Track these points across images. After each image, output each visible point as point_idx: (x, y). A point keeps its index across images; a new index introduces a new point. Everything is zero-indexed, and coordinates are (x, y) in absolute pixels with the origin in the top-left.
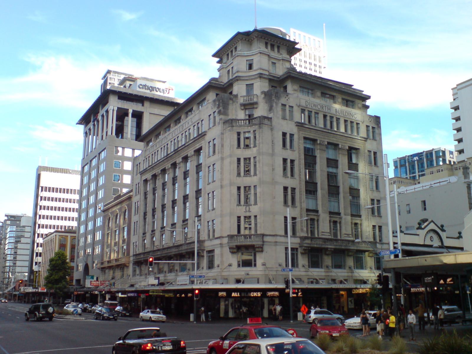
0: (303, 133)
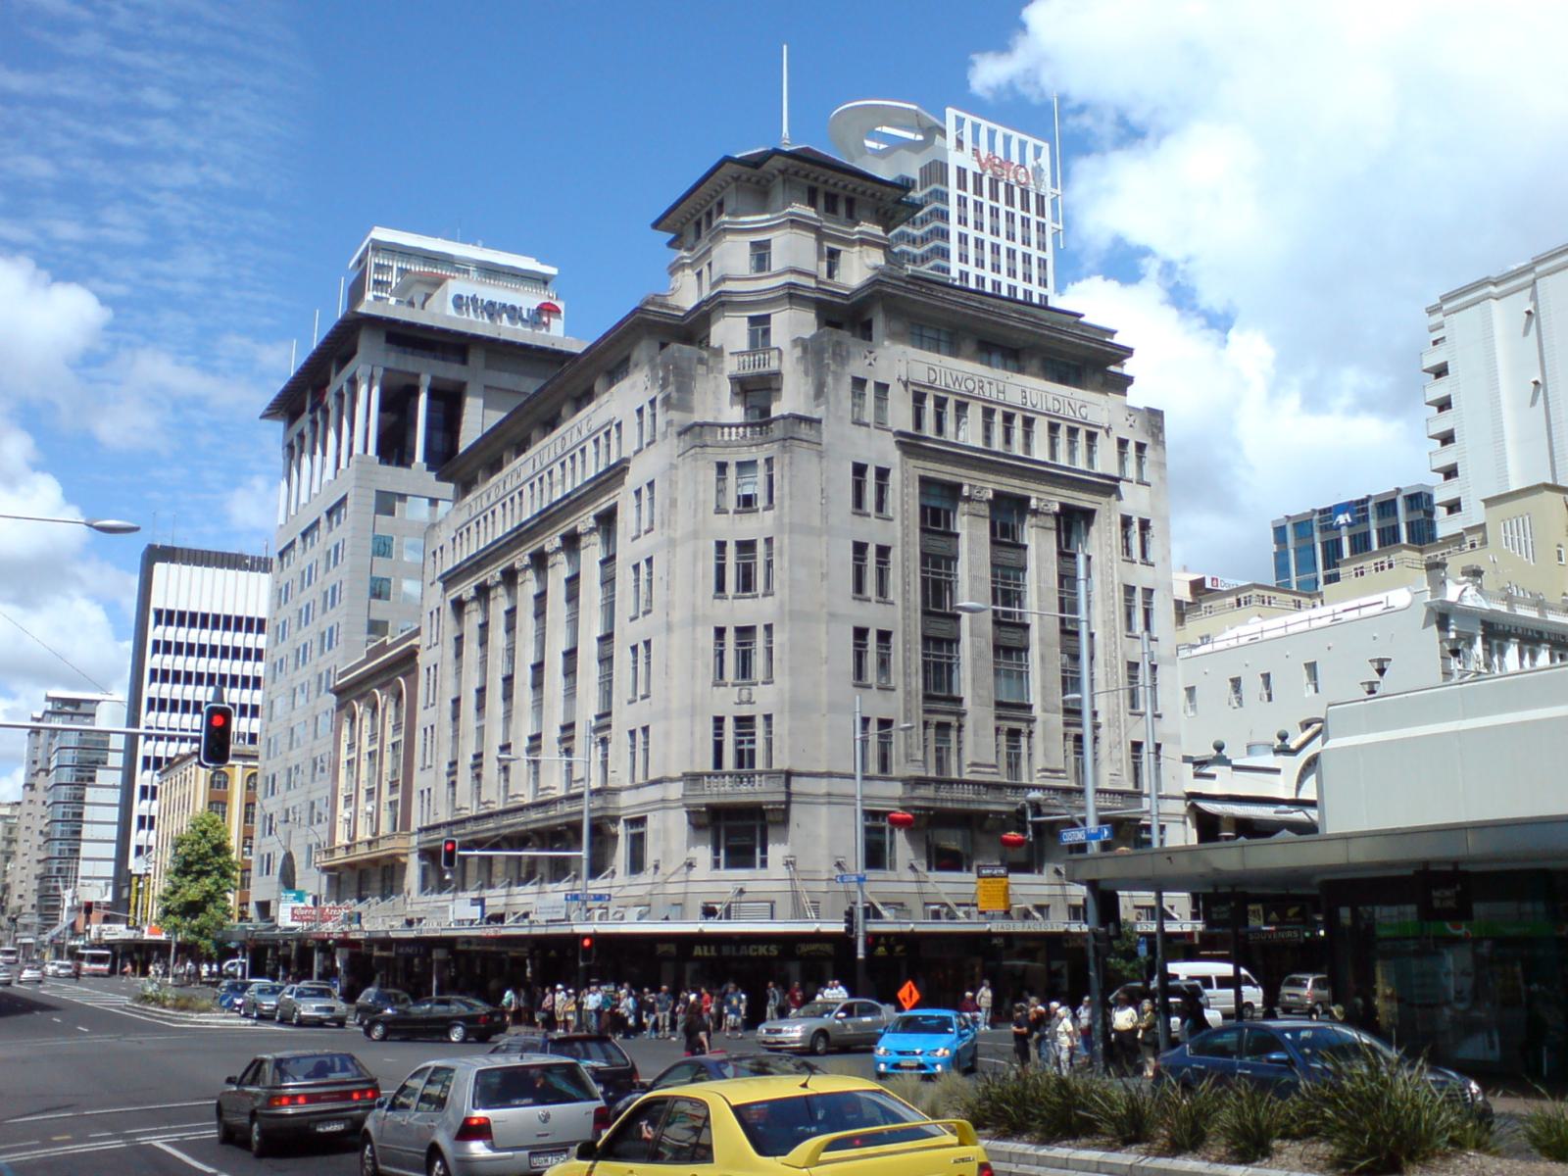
0: (920, 463)
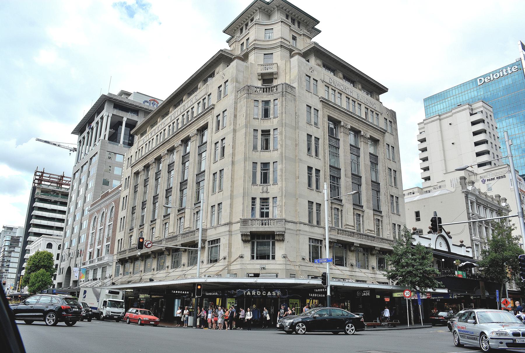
0: (328, 111)
